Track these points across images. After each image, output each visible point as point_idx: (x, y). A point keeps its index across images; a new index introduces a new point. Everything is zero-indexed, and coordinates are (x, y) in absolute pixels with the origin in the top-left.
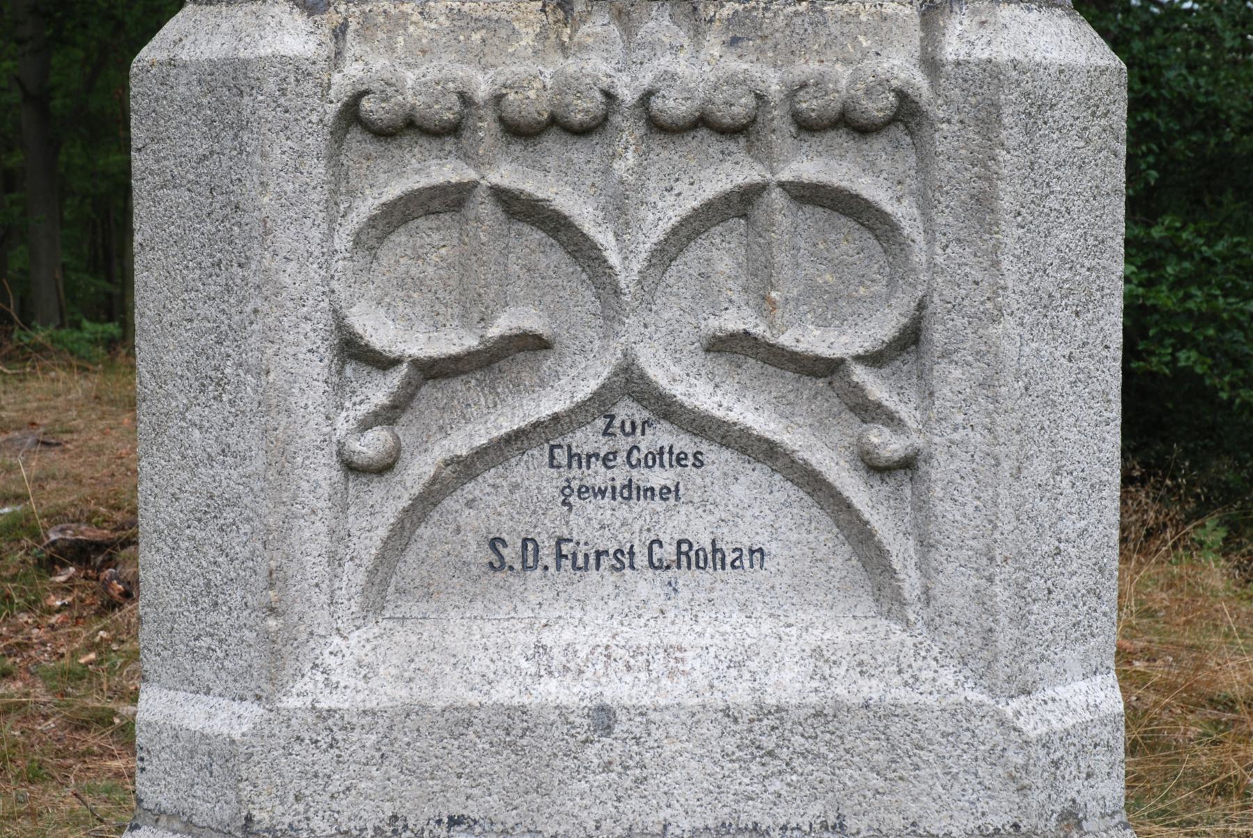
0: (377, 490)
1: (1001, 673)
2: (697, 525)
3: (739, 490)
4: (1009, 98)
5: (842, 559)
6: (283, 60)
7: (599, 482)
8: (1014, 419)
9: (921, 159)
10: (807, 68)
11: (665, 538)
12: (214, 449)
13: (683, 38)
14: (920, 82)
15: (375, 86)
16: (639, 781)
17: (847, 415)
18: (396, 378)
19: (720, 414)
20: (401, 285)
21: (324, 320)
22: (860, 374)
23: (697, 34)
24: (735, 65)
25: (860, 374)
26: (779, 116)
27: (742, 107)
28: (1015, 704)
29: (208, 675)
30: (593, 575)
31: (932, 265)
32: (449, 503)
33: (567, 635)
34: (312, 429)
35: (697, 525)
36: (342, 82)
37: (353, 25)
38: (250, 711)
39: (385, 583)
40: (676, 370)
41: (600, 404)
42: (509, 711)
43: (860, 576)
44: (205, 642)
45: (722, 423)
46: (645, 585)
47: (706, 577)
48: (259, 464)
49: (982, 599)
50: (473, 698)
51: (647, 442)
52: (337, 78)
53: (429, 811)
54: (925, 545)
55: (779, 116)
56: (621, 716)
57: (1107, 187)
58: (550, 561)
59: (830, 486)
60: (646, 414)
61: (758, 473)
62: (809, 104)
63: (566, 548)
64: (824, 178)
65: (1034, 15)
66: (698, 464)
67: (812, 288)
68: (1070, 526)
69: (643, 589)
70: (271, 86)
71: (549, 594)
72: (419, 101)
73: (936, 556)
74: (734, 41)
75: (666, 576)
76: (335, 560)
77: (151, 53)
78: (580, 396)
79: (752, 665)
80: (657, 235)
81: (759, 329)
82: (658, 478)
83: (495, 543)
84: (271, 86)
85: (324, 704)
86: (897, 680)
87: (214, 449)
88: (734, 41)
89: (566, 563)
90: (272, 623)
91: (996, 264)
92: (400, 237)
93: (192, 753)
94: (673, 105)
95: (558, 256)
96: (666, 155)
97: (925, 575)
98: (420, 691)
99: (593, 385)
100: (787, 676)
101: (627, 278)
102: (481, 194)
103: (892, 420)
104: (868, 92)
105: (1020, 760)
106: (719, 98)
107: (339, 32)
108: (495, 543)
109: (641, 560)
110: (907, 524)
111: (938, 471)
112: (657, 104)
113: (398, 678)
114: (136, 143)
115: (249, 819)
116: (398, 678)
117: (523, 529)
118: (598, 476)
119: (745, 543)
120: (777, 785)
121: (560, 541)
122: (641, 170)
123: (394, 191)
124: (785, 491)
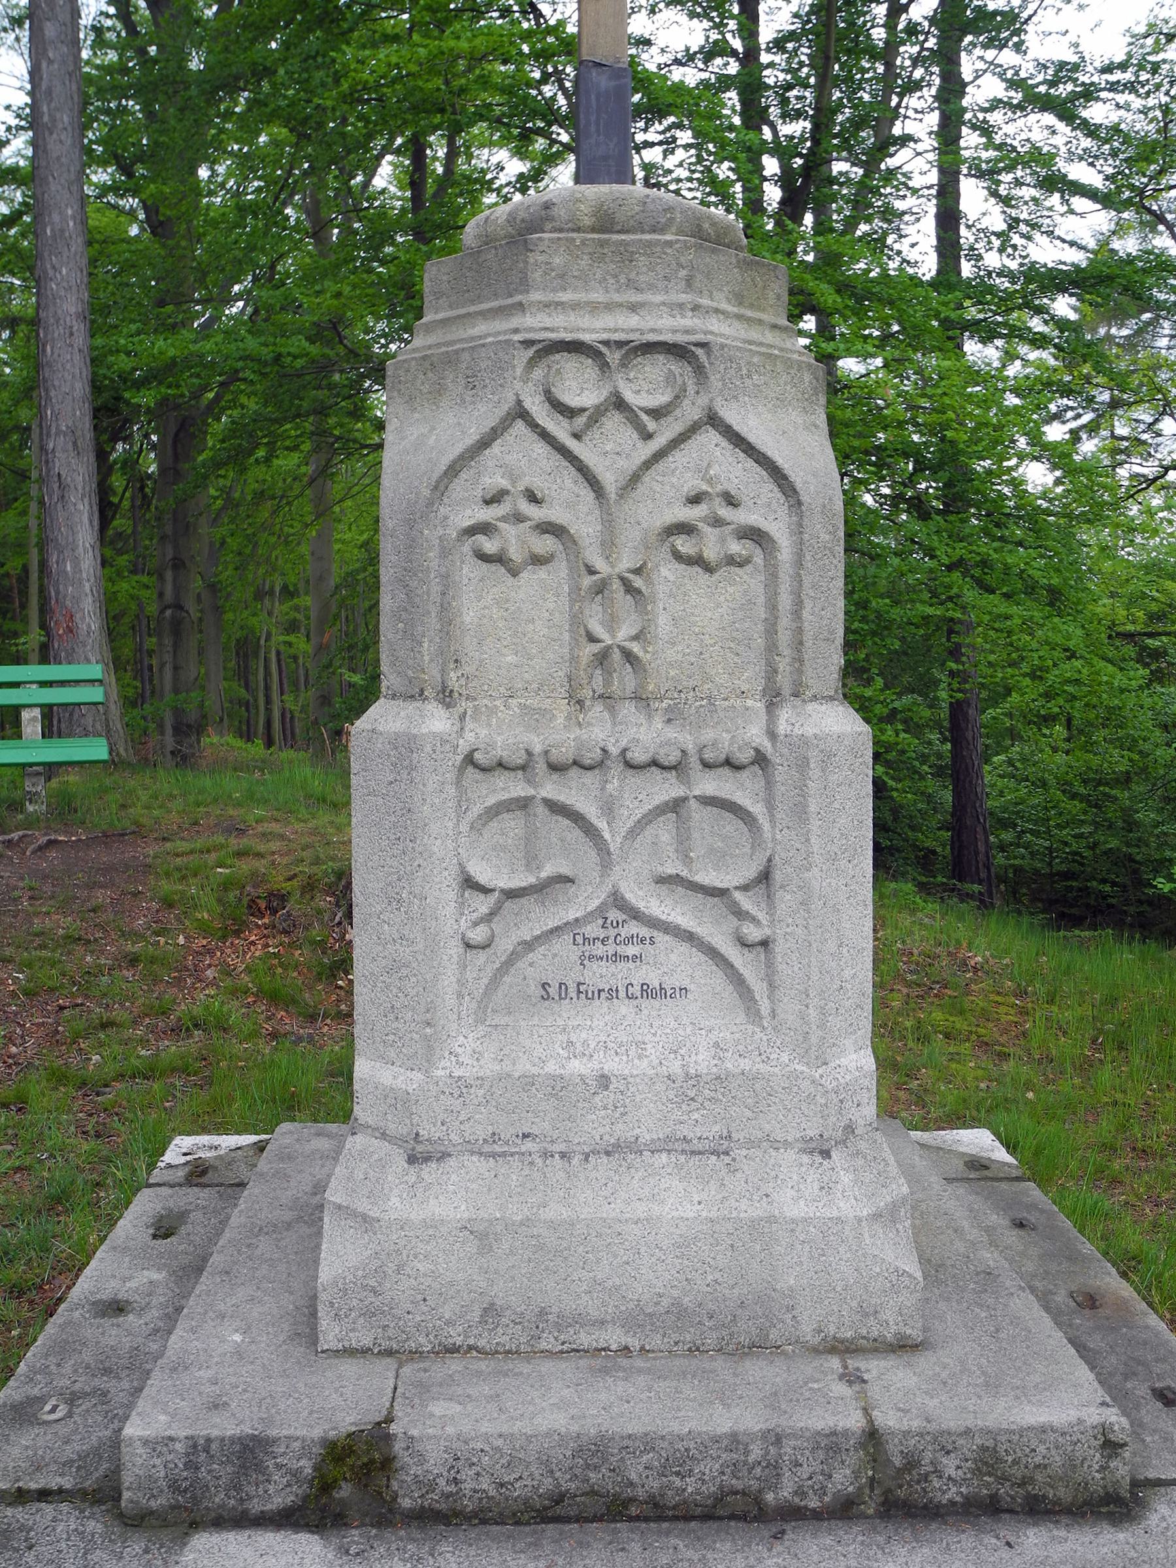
0: (481, 957)
1: (813, 1053)
2: (652, 975)
3: (673, 957)
4: (813, 755)
5: (728, 992)
6: (435, 735)
7: (599, 953)
8: (818, 922)
9: (768, 783)
10: (708, 735)
11: (635, 983)
12: (396, 936)
13: (642, 719)
14: (767, 746)
15: (482, 746)
16: (623, 1114)
17: (731, 917)
18: (493, 898)
19: (664, 917)
20: (494, 849)
21: (454, 870)
22: (738, 896)
23: (650, 717)
24: (671, 733)
25: (738, 896)
26: (694, 761)
27: (673, 757)
28: (820, 1071)
29: (393, 1055)
30: (597, 1002)
31: (774, 839)
32: (520, 964)
33: (584, 1035)
34: (449, 927)
35: (652, 975)
36: (464, 747)
37: (469, 712)
38: (418, 1076)
39: (486, 1007)
40: (640, 893)
41: (601, 911)
42: (553, 1077)
43: (738, 1002)
44: (391, 1037)
45: (664, 922)
46: (624, 1008)
47: (656, 1003)
48: (421, 946)
49: (803, 1017)
50: (535, 1070)
51: (625, 932)
52: (461, 741)
53: (512, 1131)
54: (772, 986)
55: (694, 761)
56: (613, 1079)
57: (863, 793)
58: (574, 995)
59: (722, 956)
60: (624, 917)
61: (684, 948)
62: (709, 755)
63: (582, 988)
64: (717, 794)
65: (824, 707)
66: (652, 943)
67: (712, 850)
68: (847, 973)
69: (624, 1010)
70: (428, 749)
71: (573, 1012)
72: (505, 754)
73: (778, 994)
74: (669, 720)
75: (635, 1002)
76: (460, 996)
77: (362, 724)
78: (589, 909)
79: (682, 1052)
80: (630, 824)
81: (684, 873)
82: (631, 950)
83: (544, 985)
84: (428, 749)
85: (456, 1074)
86: (758, 1059)
87: (396, 936)
88: (669, 720)
89: (583, 996)
90: (428, 1030)
91: (808, 840)
92: (494, 824)
93: (386, 1097)
94: (638, 755)
95: (577, 833)
96: (634, 780)
97: (772, 1002)
98: (507, 1067)
99: (597, 903)
100: (701, 1057)
101: (613, 839)
102: (538, 801)
103: (754, 920)
104: (740, 748)
105: (823, 1101)
106: (662, 752)
107: (462, 717)
108: (544, 985)
109: (622, 994)
110: (762, 975)
111: (779, 948)
112: (629, 755)
113: (495, 1059)
114: (353, 771)
115: (417, 1134)
116: (495, 1059)
117: (559, 978)
118: (599, 949)
119: (677, 985)
120: (696, 1116)
121: (579, 984)
122: (621, 789)
123: (491, 801)
124: (698, 957)
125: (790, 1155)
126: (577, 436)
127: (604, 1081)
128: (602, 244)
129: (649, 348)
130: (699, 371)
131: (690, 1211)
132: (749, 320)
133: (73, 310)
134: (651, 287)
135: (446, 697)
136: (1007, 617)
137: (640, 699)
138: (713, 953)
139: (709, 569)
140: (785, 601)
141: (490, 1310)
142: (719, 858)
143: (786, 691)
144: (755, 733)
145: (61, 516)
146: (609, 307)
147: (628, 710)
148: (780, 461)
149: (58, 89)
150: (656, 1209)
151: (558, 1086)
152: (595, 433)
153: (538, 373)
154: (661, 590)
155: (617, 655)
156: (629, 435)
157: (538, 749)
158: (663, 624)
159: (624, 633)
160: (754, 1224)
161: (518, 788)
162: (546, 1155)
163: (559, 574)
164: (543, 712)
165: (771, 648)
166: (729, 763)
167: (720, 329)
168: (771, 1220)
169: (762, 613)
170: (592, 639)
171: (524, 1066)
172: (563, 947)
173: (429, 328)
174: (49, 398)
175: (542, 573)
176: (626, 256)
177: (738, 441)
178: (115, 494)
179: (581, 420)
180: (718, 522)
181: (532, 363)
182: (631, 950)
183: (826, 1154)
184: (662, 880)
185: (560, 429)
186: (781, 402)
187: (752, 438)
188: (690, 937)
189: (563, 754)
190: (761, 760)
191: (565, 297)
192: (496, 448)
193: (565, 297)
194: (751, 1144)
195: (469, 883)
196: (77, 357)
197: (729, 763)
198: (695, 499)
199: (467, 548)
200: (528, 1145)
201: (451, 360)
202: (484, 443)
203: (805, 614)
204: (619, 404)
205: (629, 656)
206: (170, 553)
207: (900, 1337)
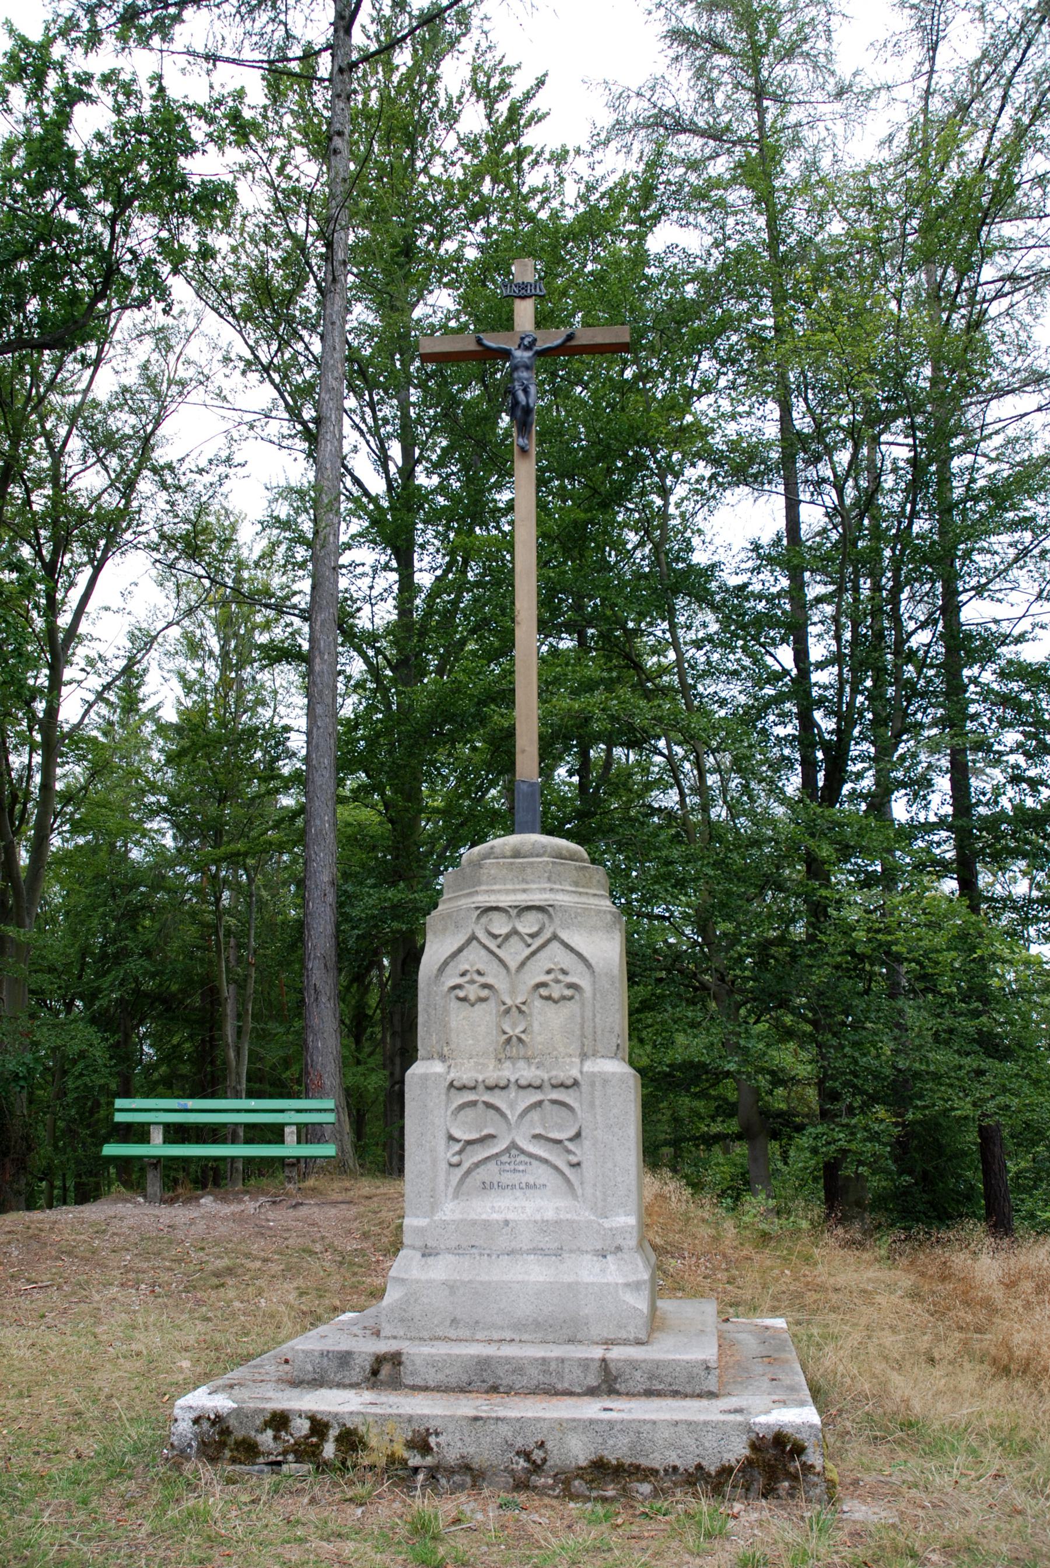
5: (564, 1187)
10: (554, 1073)
14: (579, 1077)
18: (461, 1144)
21: (444, 1131)
22: (567, 1143)
24: (538, 1073)
25: (567, 1143)
26: (546, 1084)
27: (538, 1083)
36: (449, 1078)
38: (427, 1220)
41: (507, 1150)
46: (518, 1193)
51: (518, 1159)
54: (582, 1183)
62: (554, 1082)
77: (409, 1072)
81: (543, 1133)
82: (521, 1168)
92: (462, 1113)
94: (523, 1082)
96: (522, 1093)
98: (465, 1216)
118: (507, 1167)
123: (461, 1102)
124: (551, 1171)
125: (589, 1257)
126: (499, 947)
127: (507, 1223)
128: (512, 864)
129: (529, 908)
130: (550, 916)
131: (541, 1279)
132: (580, 893)
133: (326, 879)
134: (533, 882)
135: (443, 1058)
136: (960, 1067)
137: (527, 1059)
138: (556, 1168)
139: (556, 1002)
140: (589, 1014)
141: (454, 1321)
142: (561, 1128)
143: (590, 1053)
144: (575, 1073)
145: (315, 1010)
146: (514, 891)
147: (521, 1064)
148: (585, 954)
149: (322, 743)
150: (526, 1278)
151: (486, 1224)
152: (507, 944)
153: (484, 920)
154: (535, 1011)
155: (514, 1039)
156: (522, 945)
157: (480, 1079)
158: (536, 1026)
159: (520, 1028)
160: (570, 1285)
161: (471, 1097)
162: (481, 1255)
163: (491, 1006)
164: (483, 1065)
165: (583, 1036)
166: (562, 1085)
167: (562, 899)
168: (577, 1283)
169: (579, 1020)
170: (505, 1033)
171: (473, 1216)
172: (492, 1166)
173: (444, 902)
174: (310, 935)
175: (484, 1005)
176: (523, 868)
177: (567, 946)
178: (370, 1007)
179: (500, 939)
180: (558, 981)
181: (479, 917)
182: (521, 1168)
183: (605, 1257)
184: (537, 1137)
185: (492, 945)
186: (594, 928)
187: (573, 945)
188: (546, 1161)
189: (491, 1082)
190: (576, 1083)
191: (495, 887)
192: (465, 953)
193: (495, 887)
194: (571, 1251)
195: (451, 1138)
196: (328, 909)
197: (562, 1085)
198: (549, 972)
199: (452, 995)
200: (474, 1250)
201: (449, 915)
202: (460, 950)
203: (597, 1020)
204: (514, 932)
205: (520, 1040)
206: (398, 1045)
207: (636, 1338)
